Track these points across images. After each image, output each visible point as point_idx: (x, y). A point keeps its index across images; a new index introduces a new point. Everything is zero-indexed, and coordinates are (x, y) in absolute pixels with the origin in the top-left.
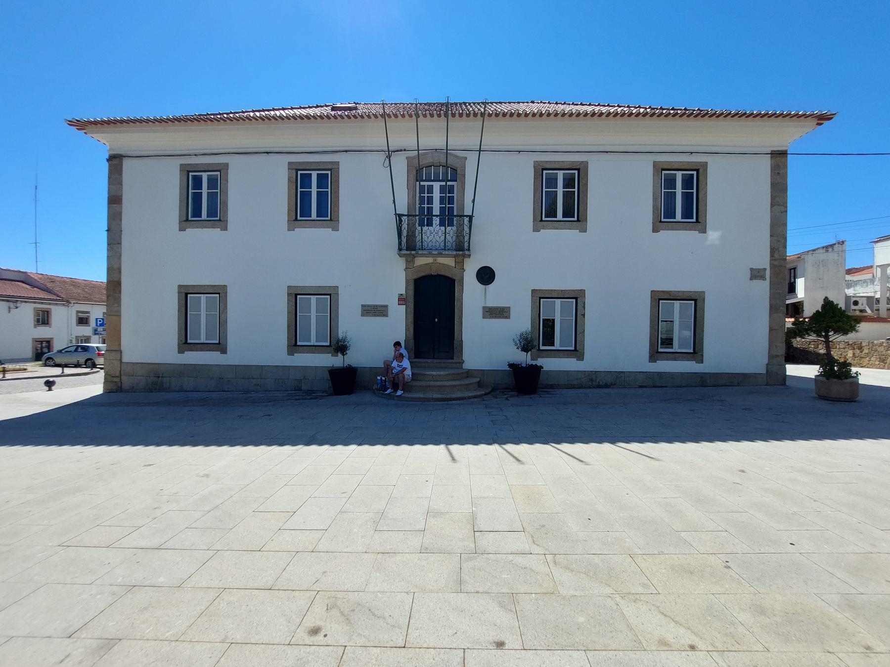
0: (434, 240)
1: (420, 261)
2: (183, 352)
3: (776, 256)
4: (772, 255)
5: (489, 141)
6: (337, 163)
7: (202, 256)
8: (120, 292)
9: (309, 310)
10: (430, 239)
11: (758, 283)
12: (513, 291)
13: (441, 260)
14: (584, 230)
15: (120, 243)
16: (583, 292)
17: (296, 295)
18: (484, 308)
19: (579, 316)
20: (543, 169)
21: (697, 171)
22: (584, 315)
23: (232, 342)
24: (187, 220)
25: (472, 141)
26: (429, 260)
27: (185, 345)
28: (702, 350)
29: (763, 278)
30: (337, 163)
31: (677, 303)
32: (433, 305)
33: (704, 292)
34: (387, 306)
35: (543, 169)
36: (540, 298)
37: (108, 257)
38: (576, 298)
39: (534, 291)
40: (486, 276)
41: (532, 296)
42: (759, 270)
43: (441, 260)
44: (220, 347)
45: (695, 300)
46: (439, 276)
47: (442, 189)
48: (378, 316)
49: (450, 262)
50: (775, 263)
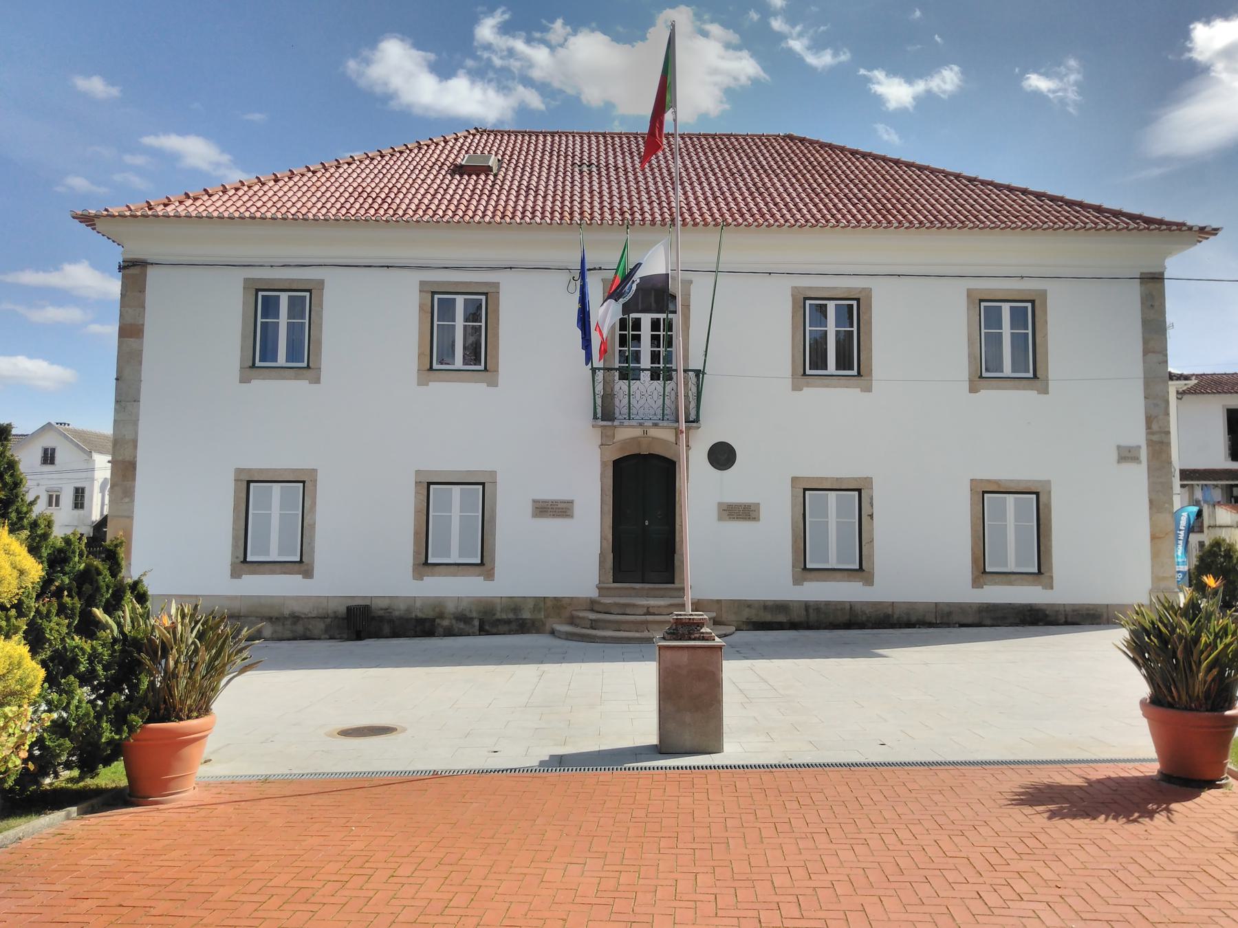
0: (646, 406)
1: (626, 433)
2: (239, 577)
3: (1155, 427)
4: (1149, 427)
5: (730, 258)
6: (497, 285)
7: (280, 422)
8: (134, 479)
9: (449, 508)
10: (642, 402)
11: (1129, 467)
12: (762, 478)
13: (654, 432)
14: (868, 389)
15: (137, 400)
16: (869, 481)
17: (249, 482)
18: (720, 504)
19: (863, 517)
20: (805, 299)
21: (1033, 302)
22: (871, 516)
23: (321, 557)
24: (253, 366)
25: (706, 258)
26: (638, 432)
27: (243, 564)
28: (1050, 569)
29: (1136, 459)
30: (497, 285)
31: (1010, 498)
32: (643, 501)
33: (1049, 482)
34: (572, 502)
35: (805, 299)
36: (805, 490)
37: (115, 421)
38: (859, 491)
39: (794, 479)
40: (722, 456)
41: (792, 487)
42: (1130, 449)
43: (654, 432)
44: (302, 566)
45: (1037, 494)
46: (651, 456)
47: (655, 325)
48: (559, 516)
49: (665, 434)
50: (1155, 438)
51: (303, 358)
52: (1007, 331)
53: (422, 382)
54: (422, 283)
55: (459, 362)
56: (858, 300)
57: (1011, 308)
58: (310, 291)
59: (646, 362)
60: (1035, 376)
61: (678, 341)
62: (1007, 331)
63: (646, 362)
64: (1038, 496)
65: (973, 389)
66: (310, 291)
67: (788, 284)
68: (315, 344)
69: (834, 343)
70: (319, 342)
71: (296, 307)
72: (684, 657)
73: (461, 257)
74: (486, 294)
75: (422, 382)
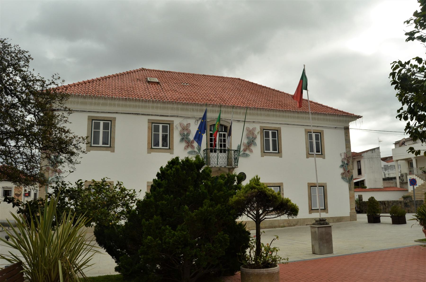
6: (173, 121)
16: (282, 184)
22: (283, 194)
38: (280, 187)
45: (323, 186)
51: (108, 144)
52: (271, 139)
53: (149, 152)
54: (89, 116)
55: (160, 146)
56: (277, 130)
57: (104, 123)
58: (111, 121)
59: (218, 147)
60: (322, 154)
61: (209, 140)
62: (271, 139)
63: (218, 147)
64: (323, 186)
65: (307, 157)
66: (111, 121)
67: (87, 115)
68: (113, 139)
69: (272, 143)
70: (114, 138)
71: (106, 127)
72: (323, 229)
73: (161, 113)
74: (169, 124)
75: (149, 152)
